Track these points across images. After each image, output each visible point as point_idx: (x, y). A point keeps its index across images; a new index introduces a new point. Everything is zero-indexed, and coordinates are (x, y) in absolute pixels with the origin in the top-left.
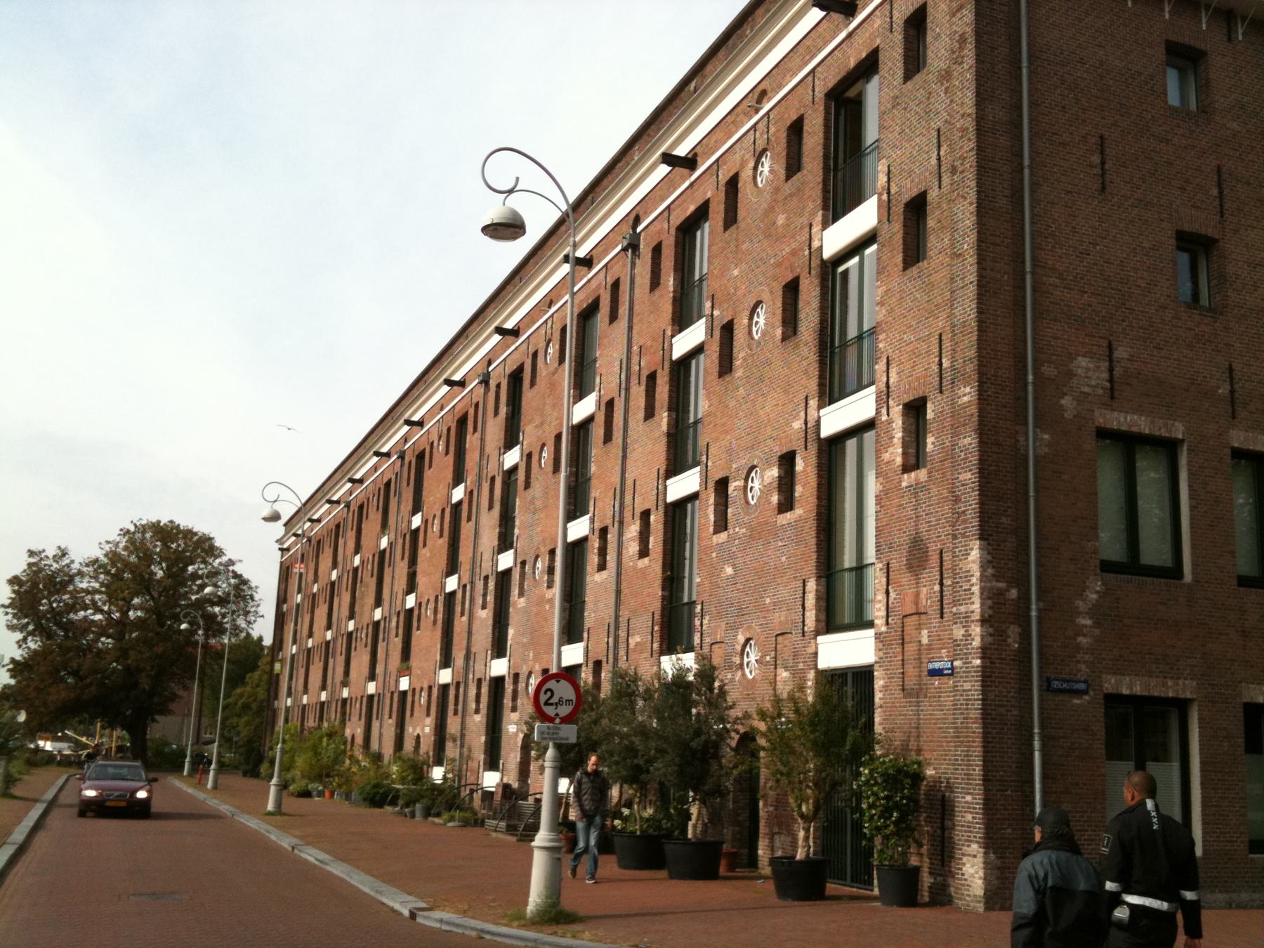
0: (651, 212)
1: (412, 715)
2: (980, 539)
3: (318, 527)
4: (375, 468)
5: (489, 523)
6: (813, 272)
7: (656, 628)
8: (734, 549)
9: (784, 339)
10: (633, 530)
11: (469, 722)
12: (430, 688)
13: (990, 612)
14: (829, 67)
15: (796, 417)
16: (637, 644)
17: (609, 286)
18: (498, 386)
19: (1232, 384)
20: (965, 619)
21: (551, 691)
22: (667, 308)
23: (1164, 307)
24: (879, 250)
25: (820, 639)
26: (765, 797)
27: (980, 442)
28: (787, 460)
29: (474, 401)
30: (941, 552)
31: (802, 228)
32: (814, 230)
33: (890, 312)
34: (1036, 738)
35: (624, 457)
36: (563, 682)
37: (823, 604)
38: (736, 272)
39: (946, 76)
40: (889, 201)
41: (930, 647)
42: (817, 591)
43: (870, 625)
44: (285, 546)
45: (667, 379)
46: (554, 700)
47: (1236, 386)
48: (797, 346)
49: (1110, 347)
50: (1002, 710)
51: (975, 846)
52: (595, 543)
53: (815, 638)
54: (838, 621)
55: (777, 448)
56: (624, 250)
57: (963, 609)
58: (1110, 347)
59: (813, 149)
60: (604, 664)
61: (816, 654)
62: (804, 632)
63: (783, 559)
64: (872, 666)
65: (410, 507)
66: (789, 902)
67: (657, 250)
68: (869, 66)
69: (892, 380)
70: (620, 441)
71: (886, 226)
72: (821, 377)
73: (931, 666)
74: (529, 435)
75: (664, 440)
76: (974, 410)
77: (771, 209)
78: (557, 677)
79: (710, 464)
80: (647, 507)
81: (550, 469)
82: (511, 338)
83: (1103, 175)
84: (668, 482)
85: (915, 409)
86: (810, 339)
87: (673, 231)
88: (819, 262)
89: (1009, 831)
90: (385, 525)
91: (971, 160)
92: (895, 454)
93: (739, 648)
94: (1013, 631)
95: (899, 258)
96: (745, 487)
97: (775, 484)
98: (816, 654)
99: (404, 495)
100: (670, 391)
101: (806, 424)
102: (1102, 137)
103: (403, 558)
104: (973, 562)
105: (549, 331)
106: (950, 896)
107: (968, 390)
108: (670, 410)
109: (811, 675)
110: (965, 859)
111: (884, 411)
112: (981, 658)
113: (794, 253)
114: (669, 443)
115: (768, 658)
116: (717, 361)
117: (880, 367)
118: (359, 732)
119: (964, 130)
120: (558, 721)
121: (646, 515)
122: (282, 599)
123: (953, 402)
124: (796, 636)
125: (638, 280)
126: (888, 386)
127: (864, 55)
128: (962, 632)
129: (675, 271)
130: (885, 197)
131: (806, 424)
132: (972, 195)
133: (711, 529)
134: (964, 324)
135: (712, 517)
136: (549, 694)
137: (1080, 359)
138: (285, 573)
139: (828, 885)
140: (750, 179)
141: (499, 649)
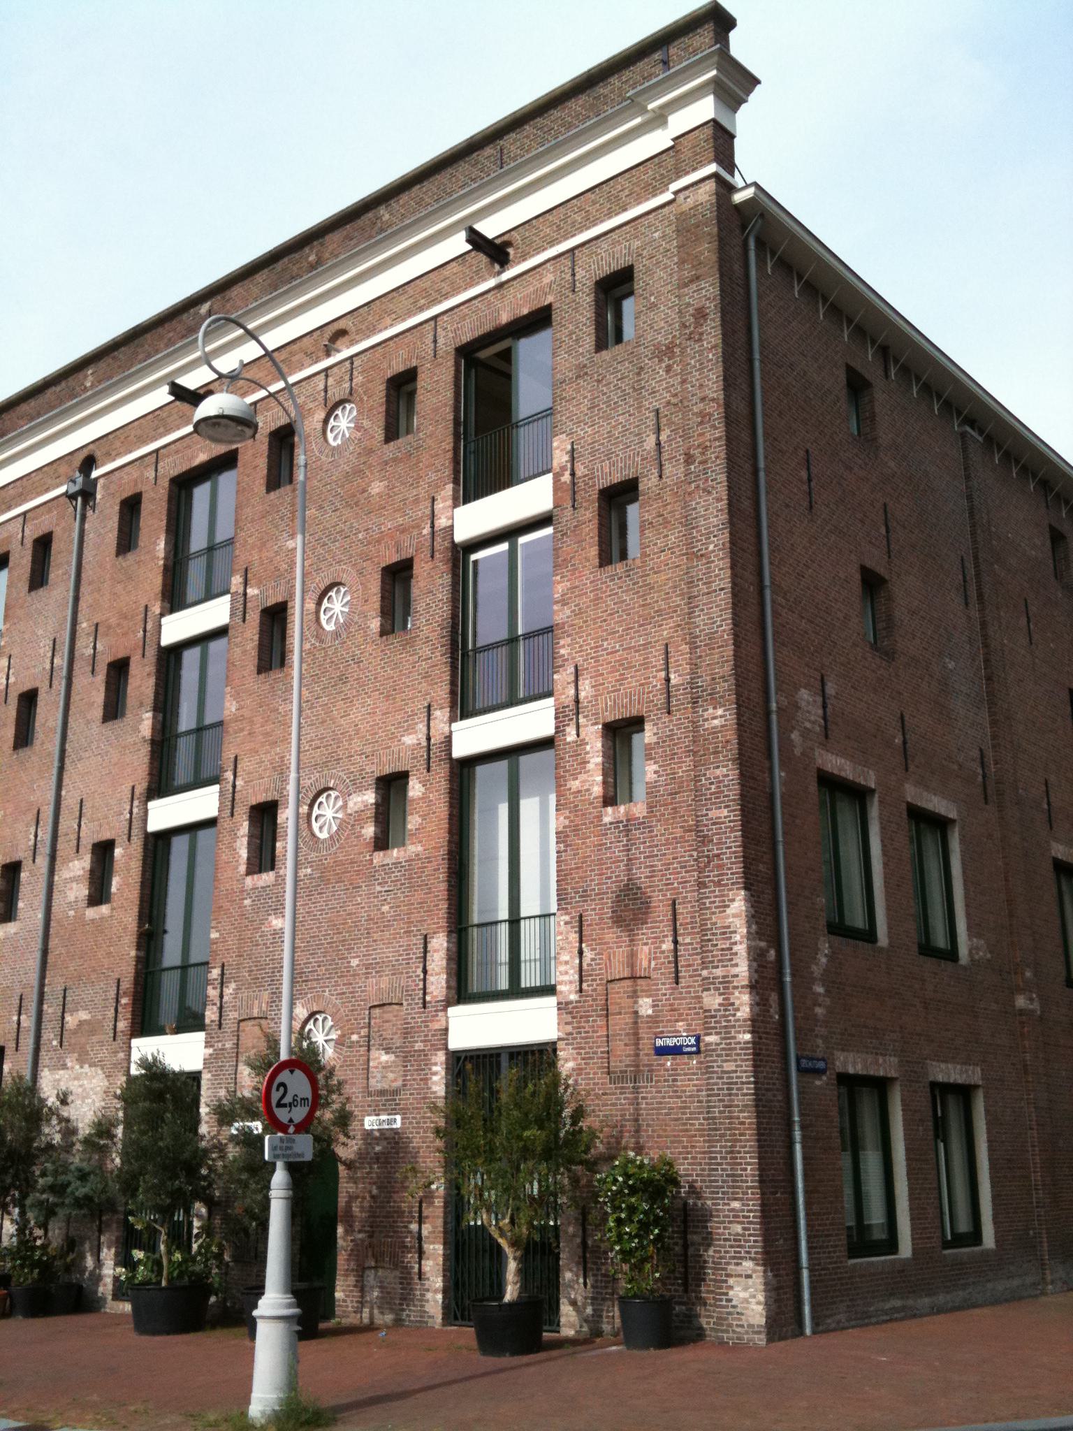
0: (119, 455)
2: (746, 888)
6: (437, 555)
7: (124, 1001)
9: (383, 633)
10: (77, 867)
14: (463, 318)
15: (410, 729)
19: (904, 734)
20: (726, 985)
21: (283, 1085)
22: (153, 580)
23: (855, 645)
25: (452, 1011)
26: (349, 1219)
30: (674, 903)
32: (439, 506)
33: (579, 613)
34: (797, 1127)
35: (61, 769)
36: (298, 1072)
41: (654, 1020)
42: (448, 949)
46: (287, 1100)
47: (908, 736)
48: (410, 642)
51: (748, 1265)
53: (445, 1009)
54: (475, 986)
56: (71, 497)
57: (719, 972)
59: (436, 410)
61: (447, 1029)
62: (424, 1003)
63: (386, 908)
64: (553, 1044)
66: (507, 1360)
67: (131, 507)
69: (582, 695)
71: (569, 512)
72: (453, 683)
73: (659, 1043)
75: (145, 750)
76: (732, 736)
77: (358, 472)
78: (290, 1065)
79: (239, 783)
84: (151, 805)
85: (620, 733)
88: (447, 544)
89: (781, 1242)
92: (593, 780)
94: (774, 997)
97: (371, 813)
100: (157, 685)
102: (807, 451)
104: (735, 916)
106: (701, 1328)
107: (720, 712)
108: (156, 709)
109: (441, 1057)
110: (731, 1281)
112: (752, 1032)
113: (403, 530)
114: (153, 752)
115: (355, 1037)
116: (254, 653)
120: (291, 1129)
124: (410, 1010)
125: (90, 537)
126: (577, 701)
127: (525, 311)
128: (719, 1000)
129: (168, 531)
130: (566, 477)
132: (722, 490)
133: (243, 869)
135: (244, 853)
136: (282, 1089)
137: (803, 690)
139: (544, 1334)
140: (319, 434)
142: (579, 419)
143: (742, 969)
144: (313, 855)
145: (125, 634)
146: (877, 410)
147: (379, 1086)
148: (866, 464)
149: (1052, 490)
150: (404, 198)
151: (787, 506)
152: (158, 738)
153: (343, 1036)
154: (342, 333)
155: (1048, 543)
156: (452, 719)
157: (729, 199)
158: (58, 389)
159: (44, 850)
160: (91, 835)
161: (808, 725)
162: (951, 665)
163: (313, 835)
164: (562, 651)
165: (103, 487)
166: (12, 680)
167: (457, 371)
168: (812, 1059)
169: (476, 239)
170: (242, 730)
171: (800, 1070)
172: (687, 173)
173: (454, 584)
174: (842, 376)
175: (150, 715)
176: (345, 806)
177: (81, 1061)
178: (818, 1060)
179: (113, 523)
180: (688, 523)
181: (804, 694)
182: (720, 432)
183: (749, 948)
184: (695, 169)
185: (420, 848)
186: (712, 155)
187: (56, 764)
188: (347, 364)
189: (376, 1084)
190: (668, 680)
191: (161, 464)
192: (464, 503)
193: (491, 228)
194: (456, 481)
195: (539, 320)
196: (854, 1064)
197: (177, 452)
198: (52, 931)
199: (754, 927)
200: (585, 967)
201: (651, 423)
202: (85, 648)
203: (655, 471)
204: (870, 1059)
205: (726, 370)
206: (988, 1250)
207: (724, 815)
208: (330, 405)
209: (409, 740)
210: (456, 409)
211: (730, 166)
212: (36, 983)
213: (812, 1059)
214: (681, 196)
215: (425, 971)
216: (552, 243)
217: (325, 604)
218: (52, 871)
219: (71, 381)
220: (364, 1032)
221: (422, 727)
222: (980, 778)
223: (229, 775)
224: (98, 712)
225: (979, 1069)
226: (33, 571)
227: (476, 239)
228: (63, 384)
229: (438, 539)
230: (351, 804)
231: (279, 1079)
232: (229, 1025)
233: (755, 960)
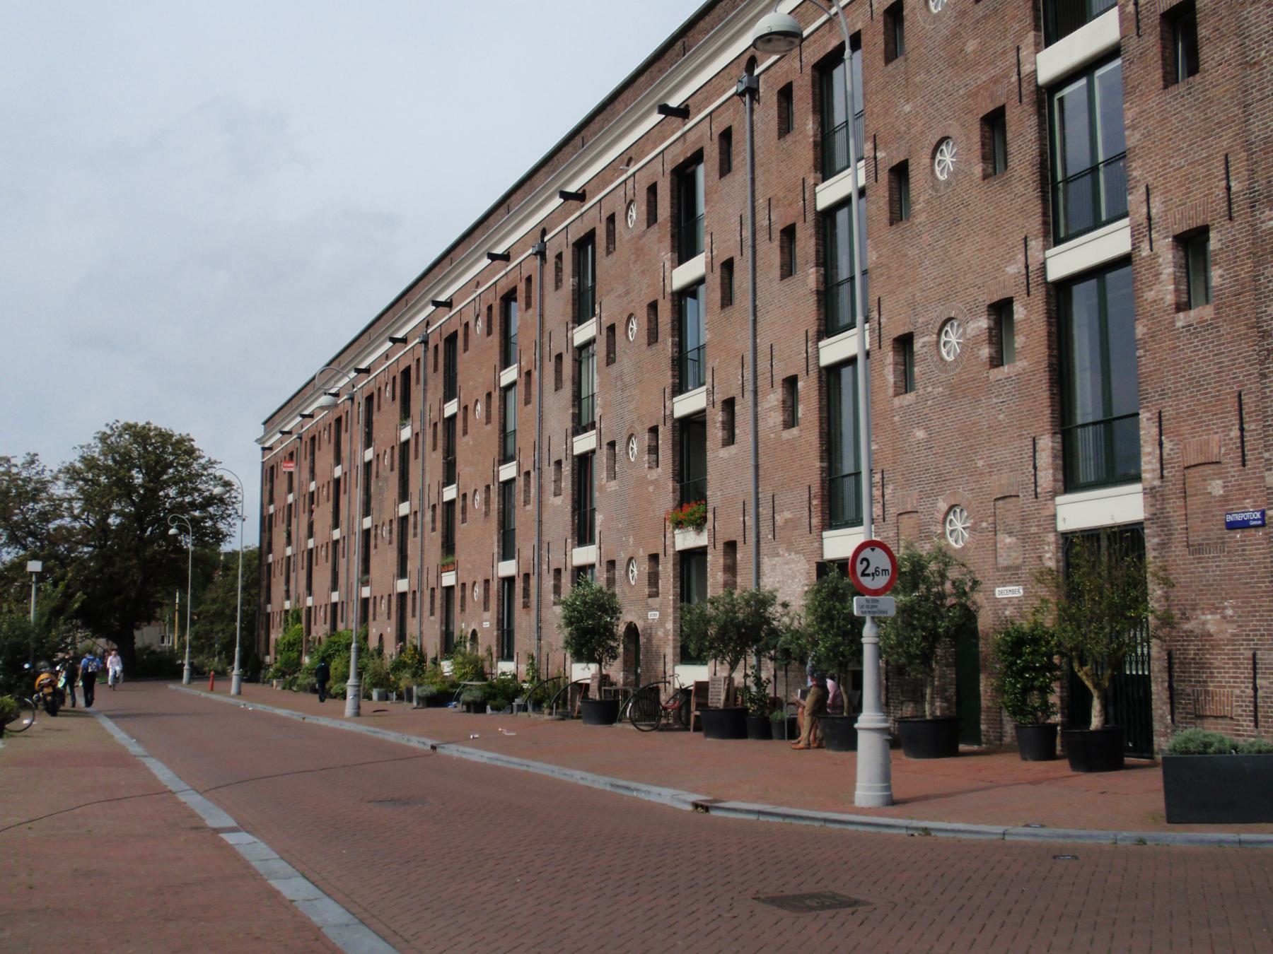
1: (463, 610)
3: (310, 423)
4: (387, 356)
5: (435, 460)
6: (1025, 100)
7: (815, 502)
11: (545, 614)
12: (487, 581)
17: (716, 137)
18: (436, 347)
22: (806, 155)
24: (1122, 66)
25: (1059, 499)
29: (525, 275)
30: (1240, 395)
31: (1004, 53)
32: (1023, 54)
38: (907, 108)
40: (1137, 13)
42: (1053, 448)
43: (1137, 478)
44: (267, 445)
45: (812, 231)
52: (521, 482)
53: (1053, 498)
56: (741, 94)
60: (740, 545)
63: (1001, 417)
65: (440, 394)
68: (698, 157)
69: (1154, 211)
70: (749, 304)
71: (1134, 41)
72: (1045, 214)
73: (1230, 518)
74: (609, 306)
75: (813, 298)
77: (956, 35)
80: (791, 372)
81: (389, 468)
82: (574, 203)
84: (821, 344)
85: (1192, 244)
86: (1025, 174)
87: (808, 70)
88: (1032, 88)
90: (406, 413)
93: (940, 517)
95: (1157, 75)
96: (938, 342)
97: (985, 336)
98: (1054, 516)
99: (431, 383)
100: (817, 244)
101: (1027, 267)
103: (435, 449)
105: (630, 193)
108: (817, 265)
109: (1051, 537)
113: (995, 80)
114: (819, 301)
115: (984, 525)
116: (886, 208)
117: (709, 373)
118: (390, 631)
121: (791, 382)
122: (269, 496)
124: (1026, 500)
125: (759, 126)
126: (1149, 218)
129: (814, 112)
131: (1027, 267)
133: (891, 391)
135: (891, 379)
138: (269, 474)
141: (583, 534)
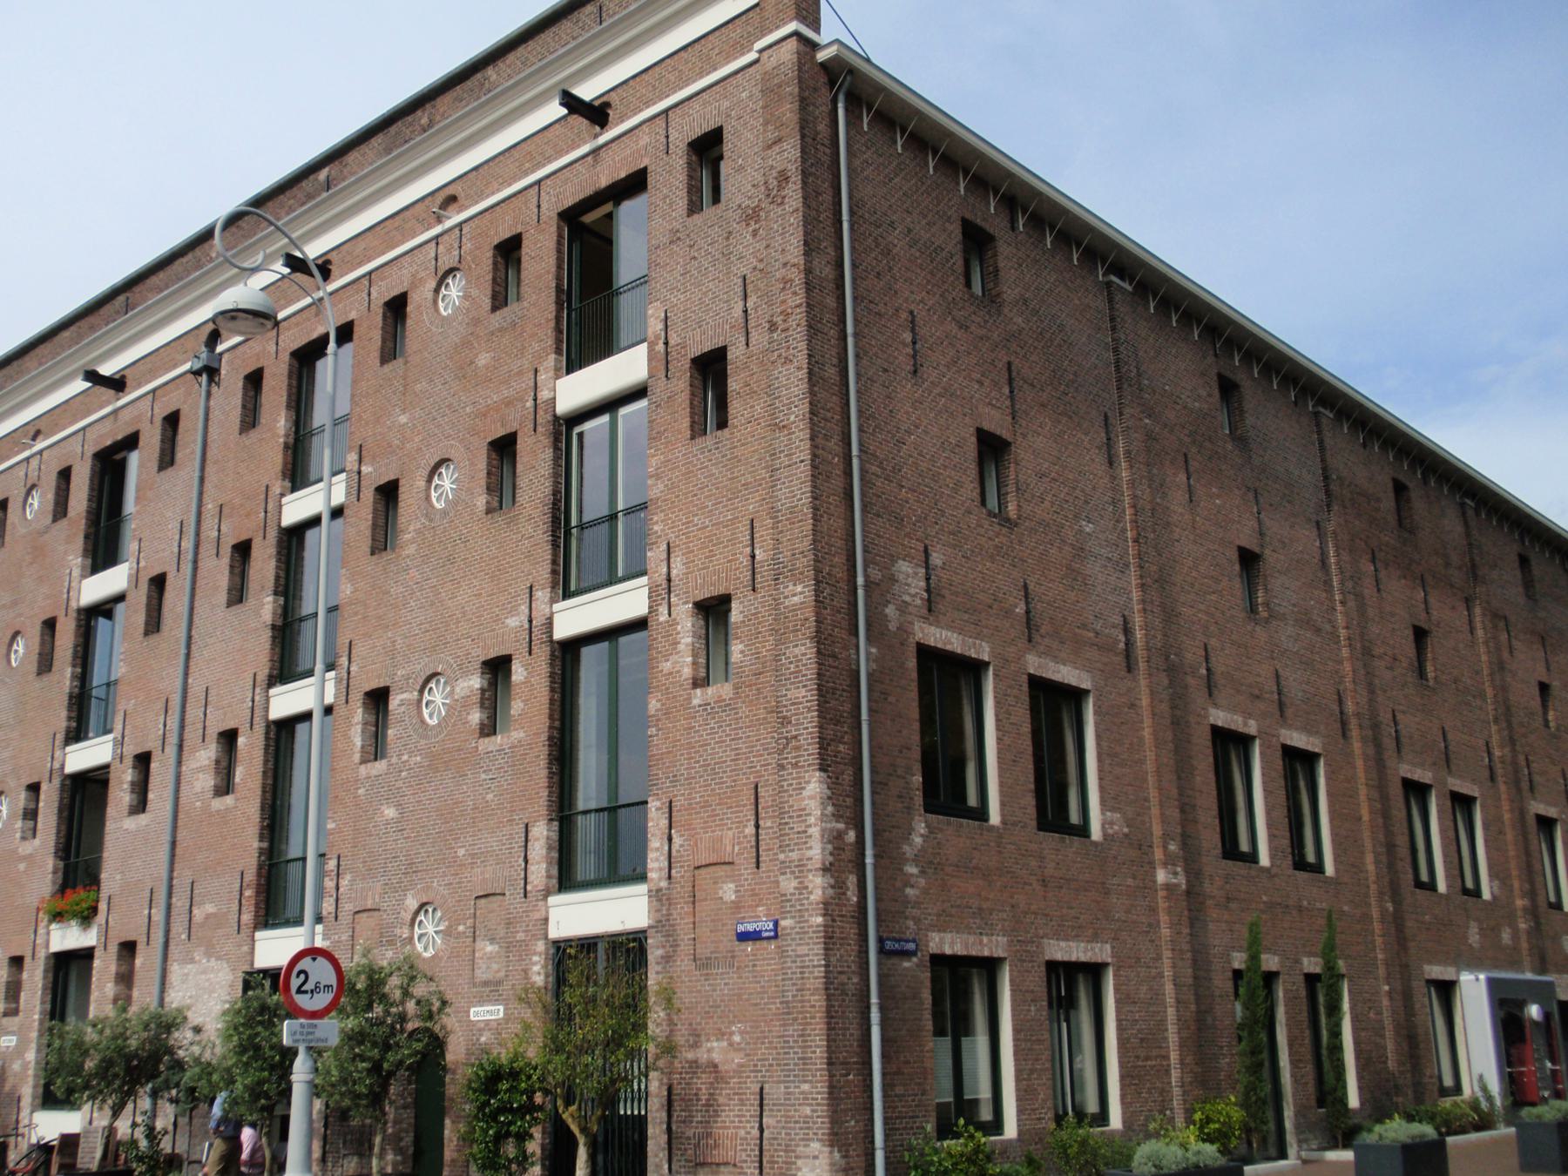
6: (540, 429)
7: (248, 893)
8: (400, 784)
9: (488, 511)
10: (205, 755)
13: (831, 859)
15: (513, 611)
16: (208, 917)
19: (1027, 603)
20: (800, 868)
22: (275, 458)
25: (552, 900)
27: (819, 652)
28: (497, 668)
31: (520, 373)
32: (542, 377)
35: (188, 656)
36: (320, 960)
37: (555, 855)
38: (403, 419)
39: (752, 215)
41: (737, 906)
43: (641, 877)
46: (309, 986)
49: (926, 551)
50: (843, 978)
53: (545, 897)
54: (579, 877)
55: (479, 651)
56: (197, 373)
57: (794, 855)
58: (926, 551)
61: (546, 920)
63: (490, 797)
64: (644, 932)
67: (254, 380)
69: (674, 572)
73: (741, 928)
75: (267, 635)
77: (466, 344)
83: (914, 357)
84: (272, 691)
85: (713, 611)
86: (536, 513)
91: (798, 318)
94: (852, 880)
97: (476, 698)
104: (811, 798)
107: (799, 588)
109: (541, 946)
110: (799, 1162)
111: (663, 610)
113: (509, 403)
114: (274, 638)
115: (461, 928)
116: (368, 533)
119: (786, 281)
123: (777, 603)
125: (215, 415)
127: (623, 175)
128: (794, 883)
129: (288, 407)
130: (660, 347)
132: (802, 358)
133: (357, 757)
134: (792, 510)
135: (358, 742)
136: (302, 977)
140: (429, 304)
142: (703, 276)
143: (816, 852)
144: (423, 742)
145: (248, 515)
146: (1001, 265)
147: (485, 977)
148: (986, 322)
149: (1220, 336)
150: (511, 57)
151: (885, 370)
152: (279, 623)
153: (450, 927)
154: (452, 199)
155: (1216, 393)
156: (553, 601)
157: (814, 57)
158: (184, 260)
159: (173, 739)
160: (217, 725)
161: (907, 598)
162: (1089, 528)
163: (423, 722)
164: (656, 528)
165: (231, 362)
166: (142, 564)
167: (560, 236)
168: (899, 940)
169: (573, 104)
170: (356, 614)
171: (882, 951)
172: (771, 31)
173: (556, 459)
174: (956, 229)
175: (270, 599)
176: (452, 692)
177: (208, 955)
178: (907, 941)
179: (237, 400)
180: (771, 391)
181: (904, 567)
182: (800, 299)
183: (823, 830)
184: (778, 28)
185: (522, 735)
186: (792, 13)
187: (183, 651)
188: (457, 231)
189: (482, 974)
190: (753, 557)
191: (282, 337)
192: (569, 372)
193: (587, 91)
194: (558, 351)
195: (635, 184)
196: (951, 944)
197: (297, 324)
198: (180, 823)
199: (830, 808)
200: (674, 853)
201: (739, 290)
202: (210, 533)
203: (743, 339)
204: (971, 939)
205: (806, 234)
206: (1113, 1131)
207: (802, 695)
208: (440, 273)
209: (513, 622)
210: (559, 278)
211: (815, 25)
212: (165, 875)
213: (899, 940)
214: (766, 54)
215: (526, 861)
216: (648, 104)
217: (436, 480)
218: (179, 763)
219: (198, 252)
220: (470, 922)
221: (524, 609)
222: (1122, 645)
223: (344, 661)
224: (223, 597)
225: (1108, 946)
226: (162, 450)
227: (573, 104)
228: (190, 256)
229: (541, 412)
230: (458, 690)
231: (300, 966)
232: (345, 917)
233: (830, 842)
